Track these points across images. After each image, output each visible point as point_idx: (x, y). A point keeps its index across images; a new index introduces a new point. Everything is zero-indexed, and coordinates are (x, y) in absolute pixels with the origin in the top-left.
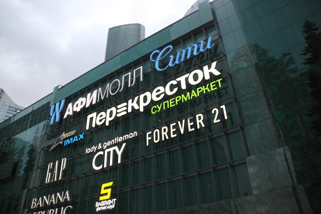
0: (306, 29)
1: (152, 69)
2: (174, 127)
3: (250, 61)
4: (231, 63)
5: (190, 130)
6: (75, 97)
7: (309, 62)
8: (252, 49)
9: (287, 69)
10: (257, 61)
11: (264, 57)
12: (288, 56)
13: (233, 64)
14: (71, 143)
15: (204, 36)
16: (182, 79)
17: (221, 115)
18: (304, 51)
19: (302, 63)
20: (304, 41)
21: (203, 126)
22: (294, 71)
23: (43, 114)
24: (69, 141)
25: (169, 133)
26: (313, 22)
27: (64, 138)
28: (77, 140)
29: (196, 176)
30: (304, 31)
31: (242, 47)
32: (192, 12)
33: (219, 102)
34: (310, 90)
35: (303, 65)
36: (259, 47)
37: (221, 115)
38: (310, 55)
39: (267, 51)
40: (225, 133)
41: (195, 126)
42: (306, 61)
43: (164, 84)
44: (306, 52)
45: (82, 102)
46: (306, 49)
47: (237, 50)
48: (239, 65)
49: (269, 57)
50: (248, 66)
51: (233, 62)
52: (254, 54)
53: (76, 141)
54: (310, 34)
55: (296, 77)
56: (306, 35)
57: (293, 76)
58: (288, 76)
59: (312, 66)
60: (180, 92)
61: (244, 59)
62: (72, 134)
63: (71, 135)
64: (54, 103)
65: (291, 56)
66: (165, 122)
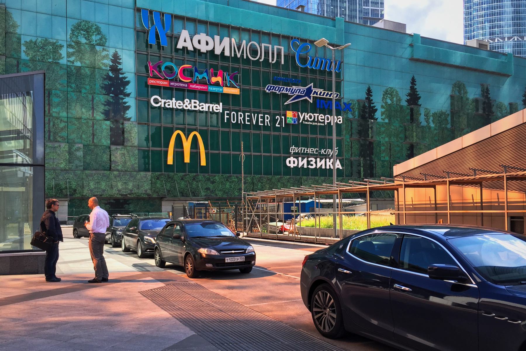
0: (113, 59)
2: (248, 116)
3: (89, 40)
13: (73, 32)
25: (244, 119)
29: (335, 173)
41: (263, 122)
47: (80, 21)
50: (86, 44)
51: (74, 30)
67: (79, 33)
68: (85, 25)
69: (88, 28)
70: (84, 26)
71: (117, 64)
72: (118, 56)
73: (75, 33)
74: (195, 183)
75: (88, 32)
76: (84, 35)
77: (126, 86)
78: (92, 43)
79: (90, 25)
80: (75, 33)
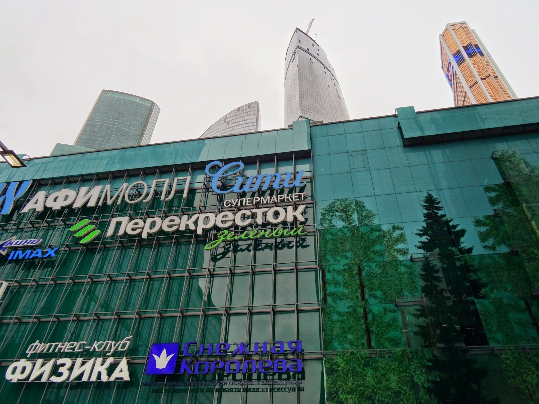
0: (427, 204)
1: (137, 192)
4: (322, 216)
6: (97, 179)
7: (424, 246)
8: (354, 206)
9: (395, 247)
10: (357, 224)
11: (368, 222)
12: (398, 230)
13: (324, 217)
14: (27, 257)
15: (274, 167)
16: (259, 212)
18: (420, 231)
19: (415, 246)
20: (423, 219)
22: (404, 252)
24: (23, 253)
26: (437, 198)
27: (13, 245)
28: (40, 255)
30: (424, 206)
31: (341, 199)
32: (220, 135)
33: (231, 268)
34: (421, 283)
35: (417, 248)
36: (363, 207)
38: (426, 239)
39: (374, 216)
40: (227, 312)
42: (421, 244)
43: (165, 217)
44: (422, 232)
45: (55, 200)
46: (423, 229)
47: (333, 201)
48: (332, 222)
49: (374, 223)
52: (356, 214)
53: (38, 257)
54: (431, 212)
55: (404, 260)
56: (426, 212)
57: (401, 258)
58: (395, 256)
59: (427, 254)
61: (340, 216)
62: (32, 243)
63: (29, 244)
64: (20, 180)
65: (403, 231)
66: (128, 273)
67: (332, 216)
68: (341, 205)
69: (346, 207)
70: (339, 206)
71: (435, 211)
72: (435, 200)
73: (327, 217)
74: (393, 385)
75: (345, 212)
76: (341, 216)
77: (460, 238)
78: (353, 224)
79: (347, 202)
80: (327, 217)
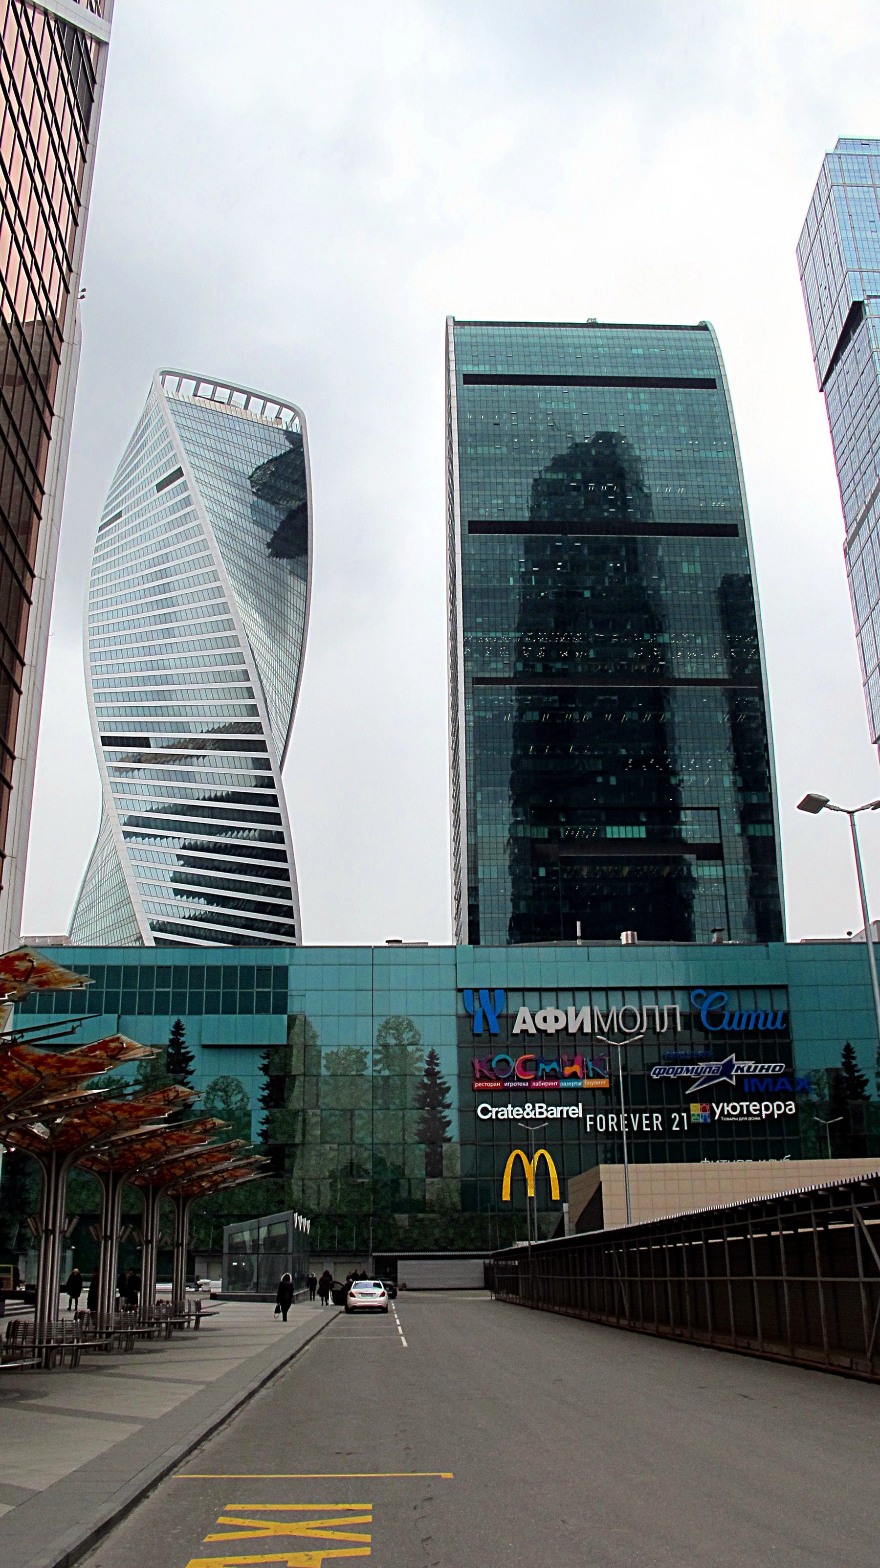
5: (645, 1129)
17: (681, 1124)
21: (661, 1129)
23: (718, 1108)
25: (618, 1124)
37: (681, 1124)
41: (650, 1125)
60: (741, 1114)
